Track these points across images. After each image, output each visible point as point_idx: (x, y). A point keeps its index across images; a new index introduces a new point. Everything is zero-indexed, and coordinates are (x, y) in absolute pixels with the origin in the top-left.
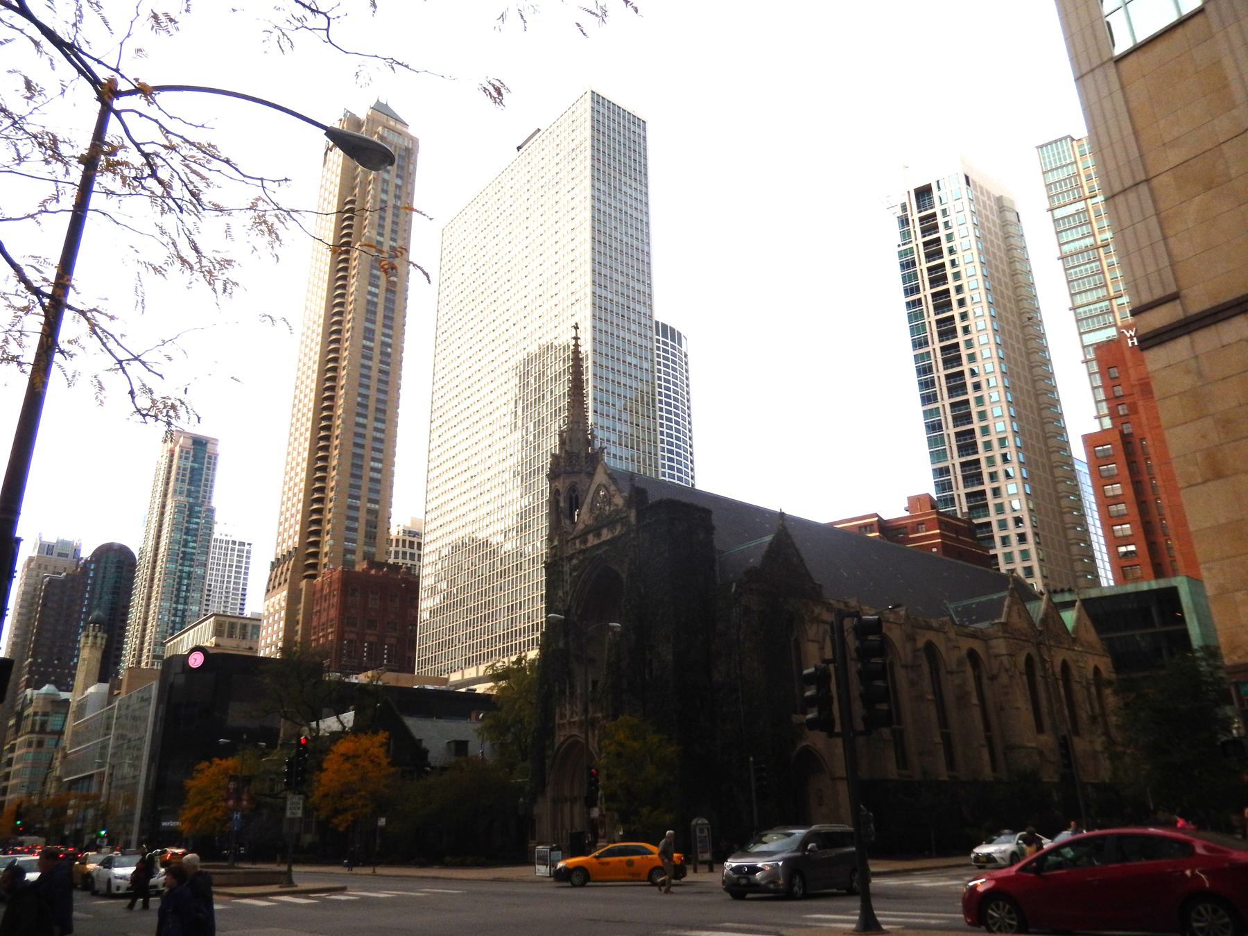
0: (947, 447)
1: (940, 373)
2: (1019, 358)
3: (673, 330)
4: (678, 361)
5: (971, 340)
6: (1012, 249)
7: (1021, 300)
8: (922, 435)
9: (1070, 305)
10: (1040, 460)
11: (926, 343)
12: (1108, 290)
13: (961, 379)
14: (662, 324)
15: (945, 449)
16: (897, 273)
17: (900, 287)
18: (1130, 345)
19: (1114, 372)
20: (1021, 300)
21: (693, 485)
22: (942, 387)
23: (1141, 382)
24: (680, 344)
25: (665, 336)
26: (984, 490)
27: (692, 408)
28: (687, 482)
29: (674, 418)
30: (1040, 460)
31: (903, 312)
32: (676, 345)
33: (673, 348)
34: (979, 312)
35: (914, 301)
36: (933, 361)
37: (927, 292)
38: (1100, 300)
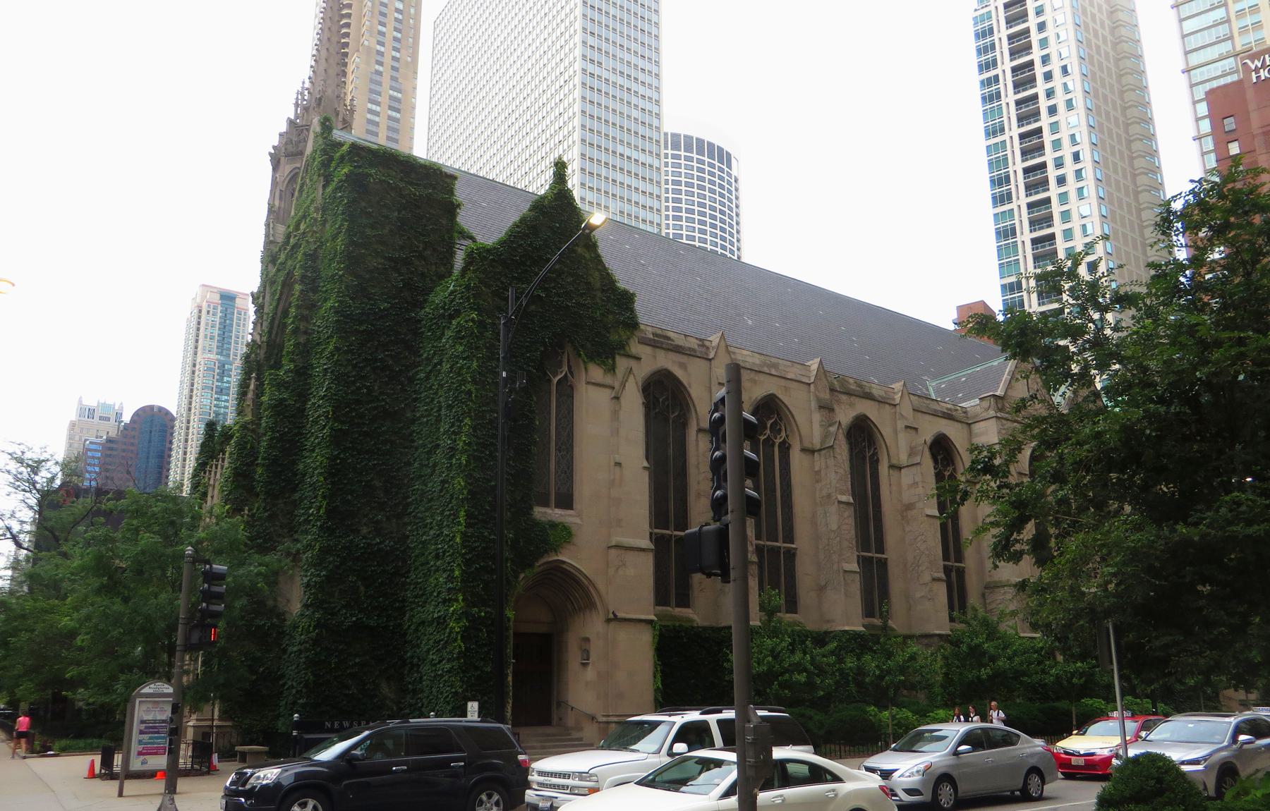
0: (1021, 257)
1: (1017, 166)
2: (1127, 216)
3: (720, 150)
4: (727, 186)
5: (1057, 122)
6: (1117, 10)
7: (1118, 26)
8: (991, 243)
9: (1183, 66)
10: (1124, 198)
11: (1002, 130)
12: (1233, 44)
13: (1048, 208)
14: (708, 143)
15: (1018, 259)
16: (971, 45)
17: (980, 126)
18: (1255, 80)
19: (1230, 124)
20: (1118, 26)
21: (739, 257)
22: (1011, 113)
23: (1264, 129)
24: (729, 166)
25: (711, 156)
26: (1028, 28)
27: (742, 224)
28: (732, 252)
29: (719, 207)
30: (1124, 198)
31: (976, 93)
32: (725, 167)
33: (721, 170)
34: (1060, 20)
35: (989, 80)
36: (1017, 222)
37: (1006, 65)
38: (1216, 25)
